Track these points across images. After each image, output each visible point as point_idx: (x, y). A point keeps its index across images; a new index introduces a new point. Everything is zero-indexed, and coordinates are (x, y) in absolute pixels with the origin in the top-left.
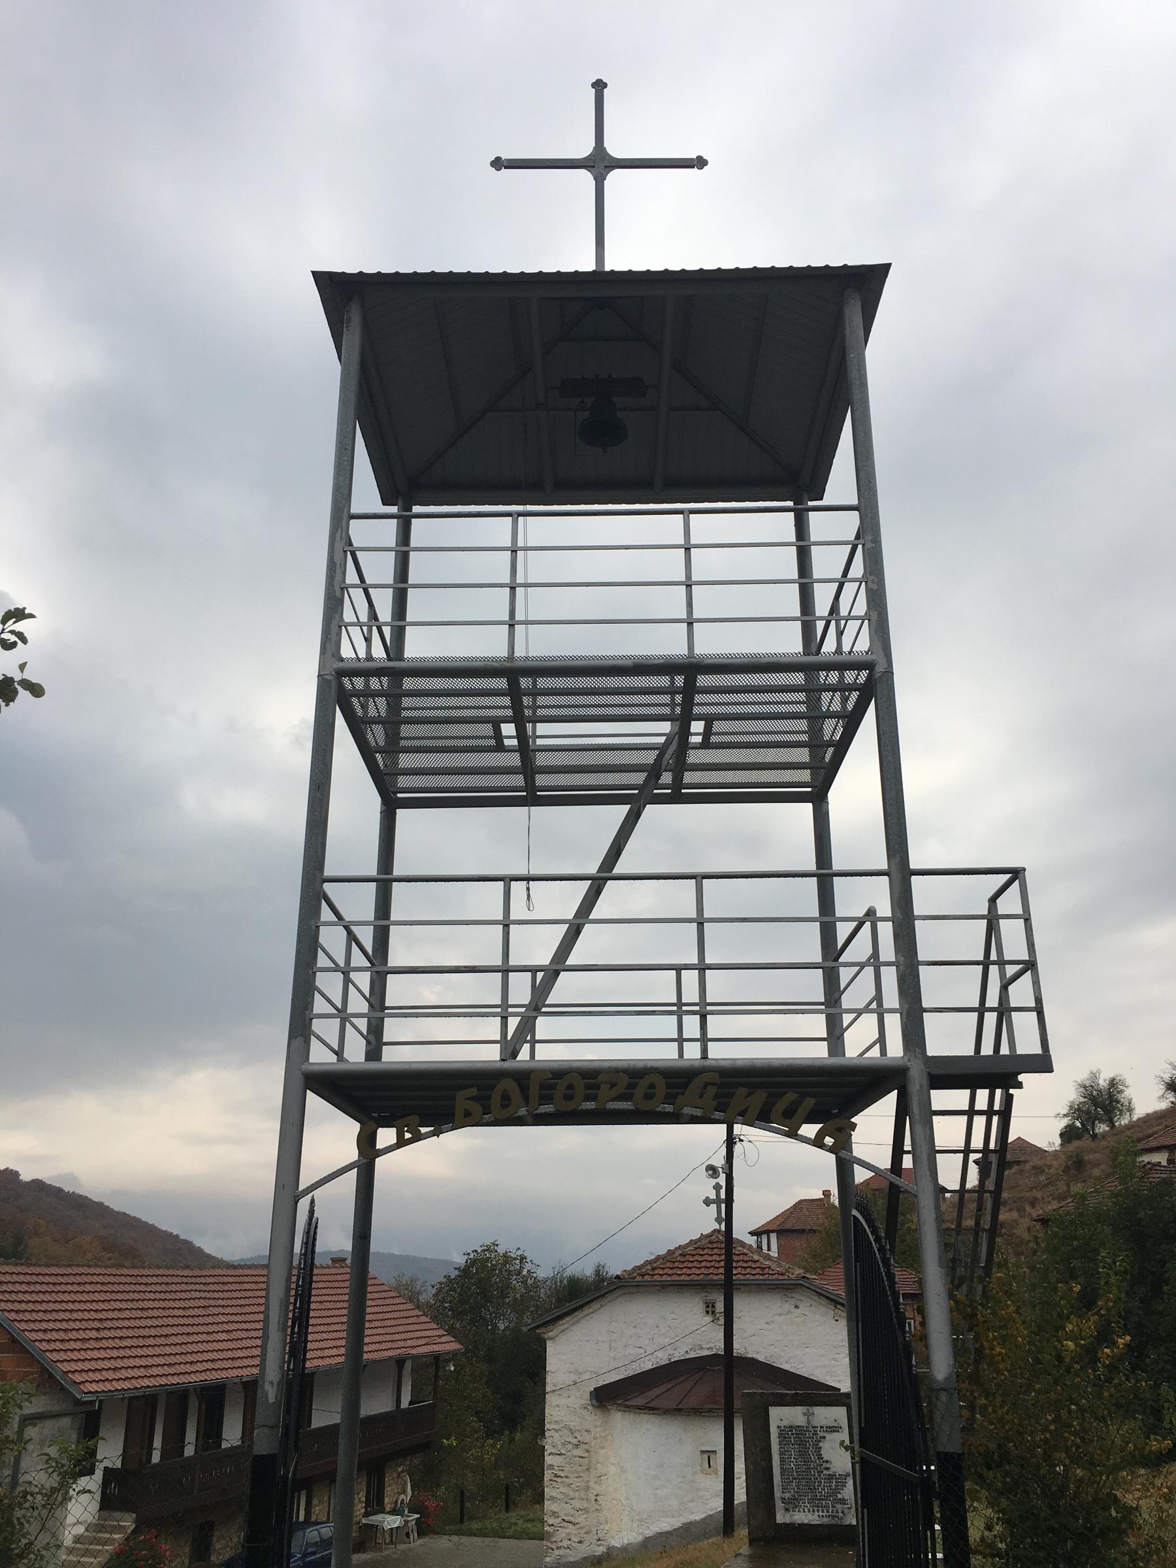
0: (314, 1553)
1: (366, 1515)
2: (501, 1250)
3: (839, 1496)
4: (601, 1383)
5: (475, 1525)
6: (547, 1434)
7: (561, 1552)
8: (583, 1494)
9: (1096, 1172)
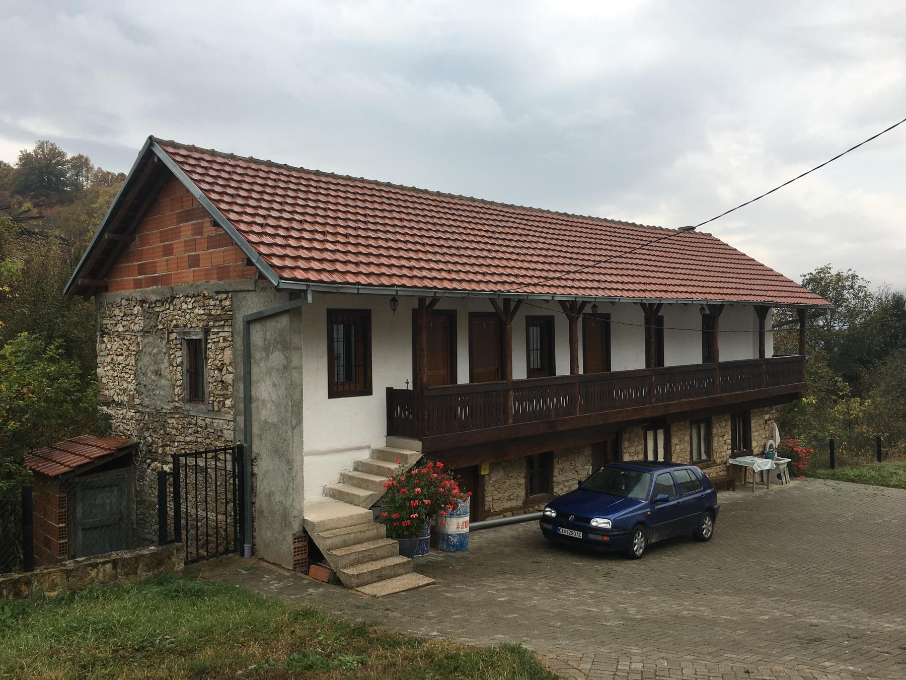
0: (665, 500)
1: (733, 456)
2: (834, 272)
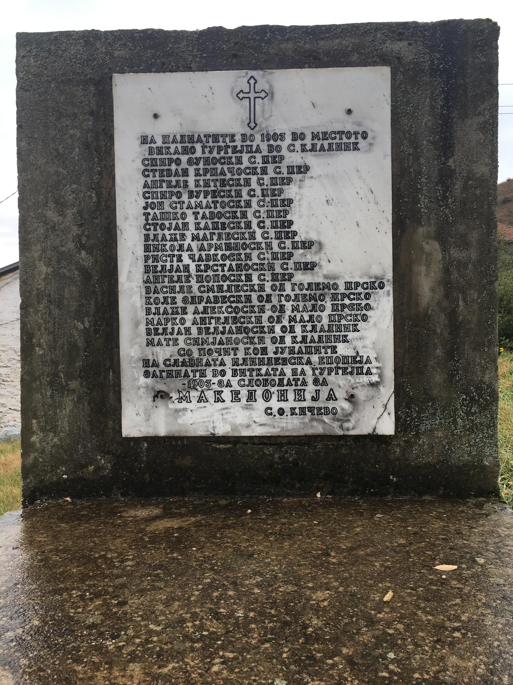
3: (342, 349)
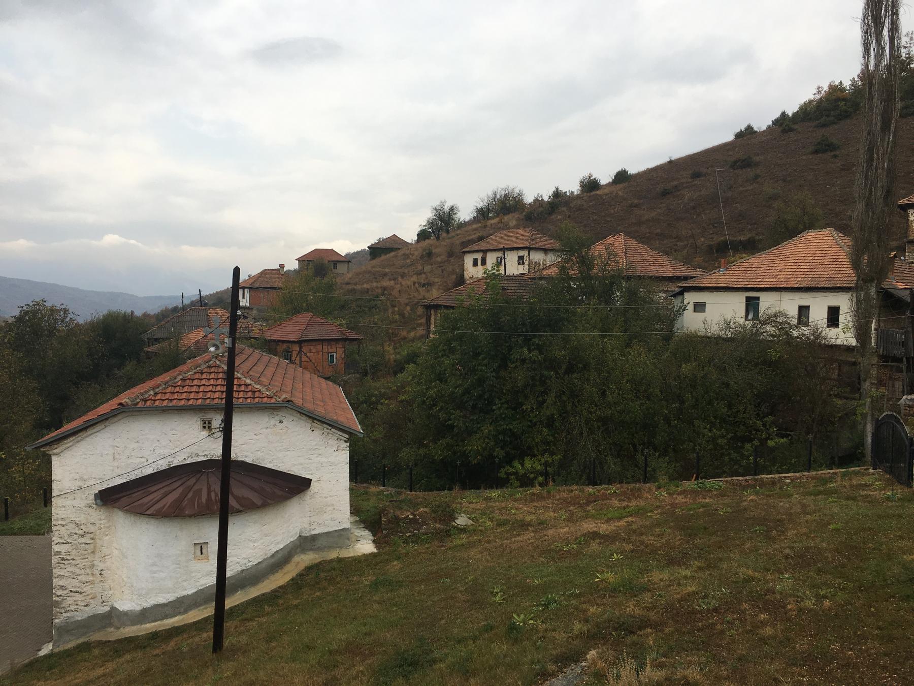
4: (105, 487)
5: (17, 524)
6: (54, 529)
7: (68, 614)
8: (88, 571)
9: (439, 259)
